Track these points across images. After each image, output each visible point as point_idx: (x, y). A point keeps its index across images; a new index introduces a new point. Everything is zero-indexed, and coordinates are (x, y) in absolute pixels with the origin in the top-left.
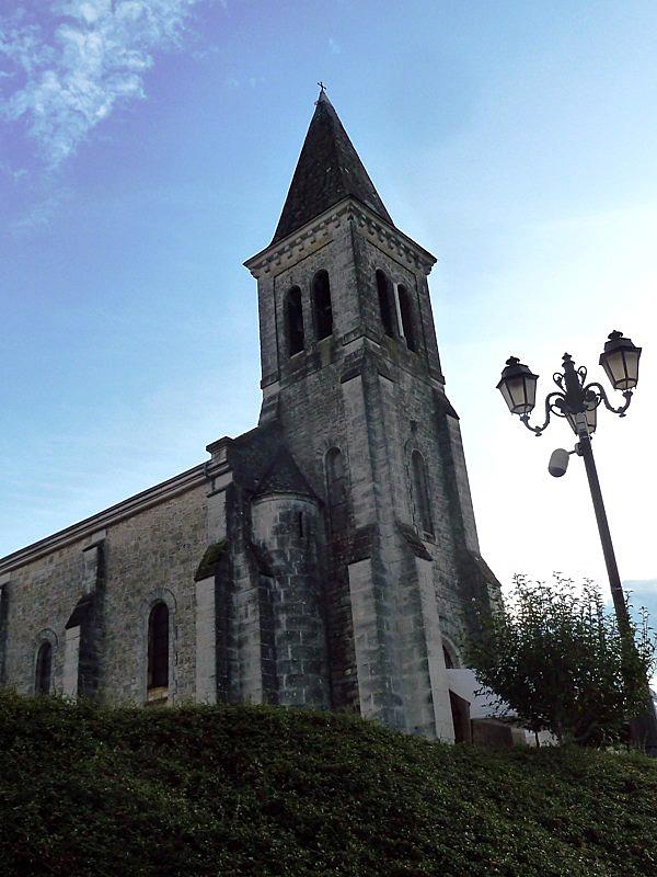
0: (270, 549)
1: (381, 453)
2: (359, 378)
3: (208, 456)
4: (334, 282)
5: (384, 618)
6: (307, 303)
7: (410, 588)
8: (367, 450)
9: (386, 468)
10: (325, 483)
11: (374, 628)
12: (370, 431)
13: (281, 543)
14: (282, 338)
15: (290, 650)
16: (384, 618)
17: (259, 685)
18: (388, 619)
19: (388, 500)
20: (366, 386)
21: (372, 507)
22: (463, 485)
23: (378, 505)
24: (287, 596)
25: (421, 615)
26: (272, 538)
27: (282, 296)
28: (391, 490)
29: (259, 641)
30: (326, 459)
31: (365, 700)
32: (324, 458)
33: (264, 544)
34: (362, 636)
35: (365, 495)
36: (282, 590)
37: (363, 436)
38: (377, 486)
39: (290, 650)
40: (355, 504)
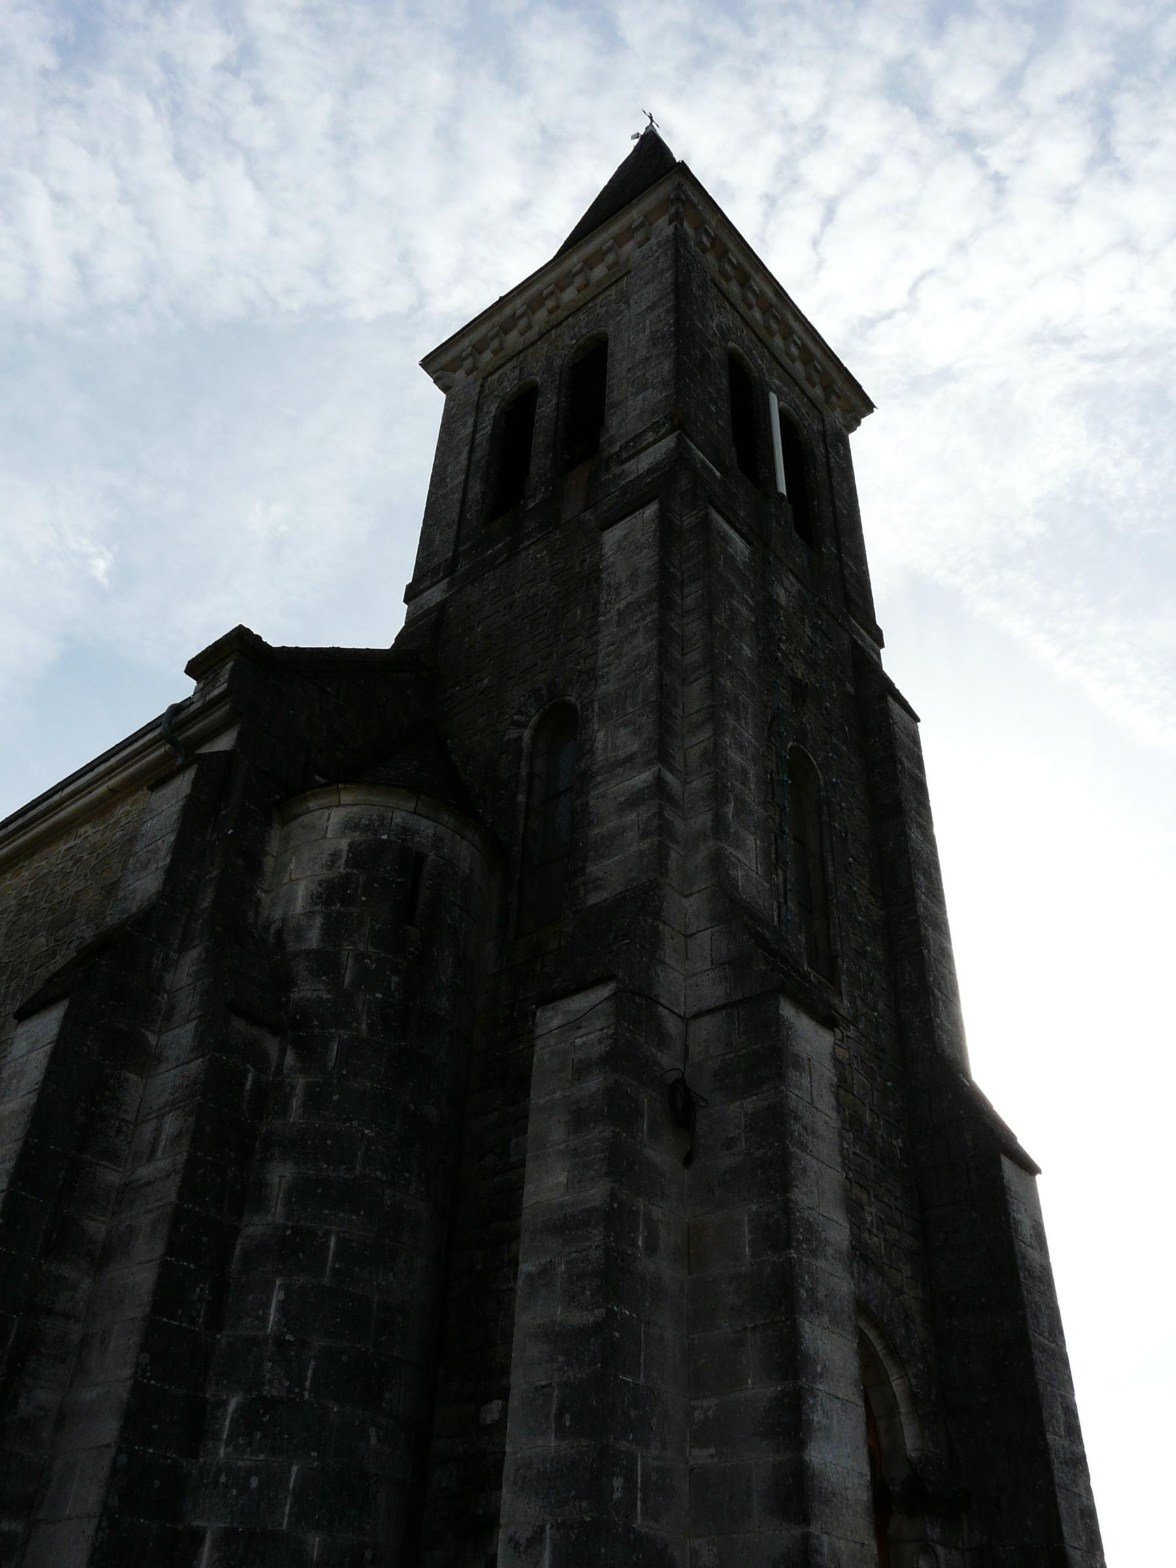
0: (292, 946)
1: (694, 698)
2: (651, 510)
3: (187, 687)
4: (619, 365)
5: (641, 1204)
6: (547, 408)
7: (751, 1104)
8: (651, 678)
9: (705, 734)
10: (521, 798)
11: (597, 1236)
12: (662, 630)
13: (334, 930)
14: (476, 487)
15: (277, 1296)
16: (641, 1204)
17: (108, 1429)
18: (657, 1212)
19: (702, 820)
20: (667, 535)
21: (644, 835)
22: (920, 826)
23: (664, 829)
24: (314, 1100)
25: (787, 1208)
26: (309, 915)
27: (493, 408)
28: (718, 792)
29: (159, 1248)
30: (534, 739)
31: (514, 1542)
32: (527, 734)
33: (280, 932)
34: (546, 1271)
35: (634, 801)
36: (301, 1082)
37: (644, 644)
38: (669, 777)
39: (277, 1296)
40: (806, 1451)
